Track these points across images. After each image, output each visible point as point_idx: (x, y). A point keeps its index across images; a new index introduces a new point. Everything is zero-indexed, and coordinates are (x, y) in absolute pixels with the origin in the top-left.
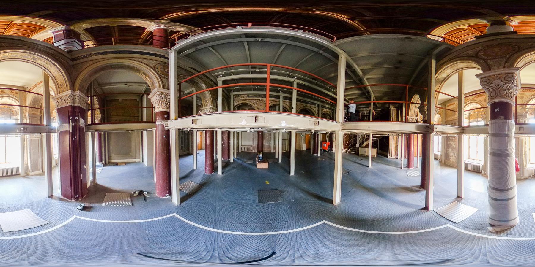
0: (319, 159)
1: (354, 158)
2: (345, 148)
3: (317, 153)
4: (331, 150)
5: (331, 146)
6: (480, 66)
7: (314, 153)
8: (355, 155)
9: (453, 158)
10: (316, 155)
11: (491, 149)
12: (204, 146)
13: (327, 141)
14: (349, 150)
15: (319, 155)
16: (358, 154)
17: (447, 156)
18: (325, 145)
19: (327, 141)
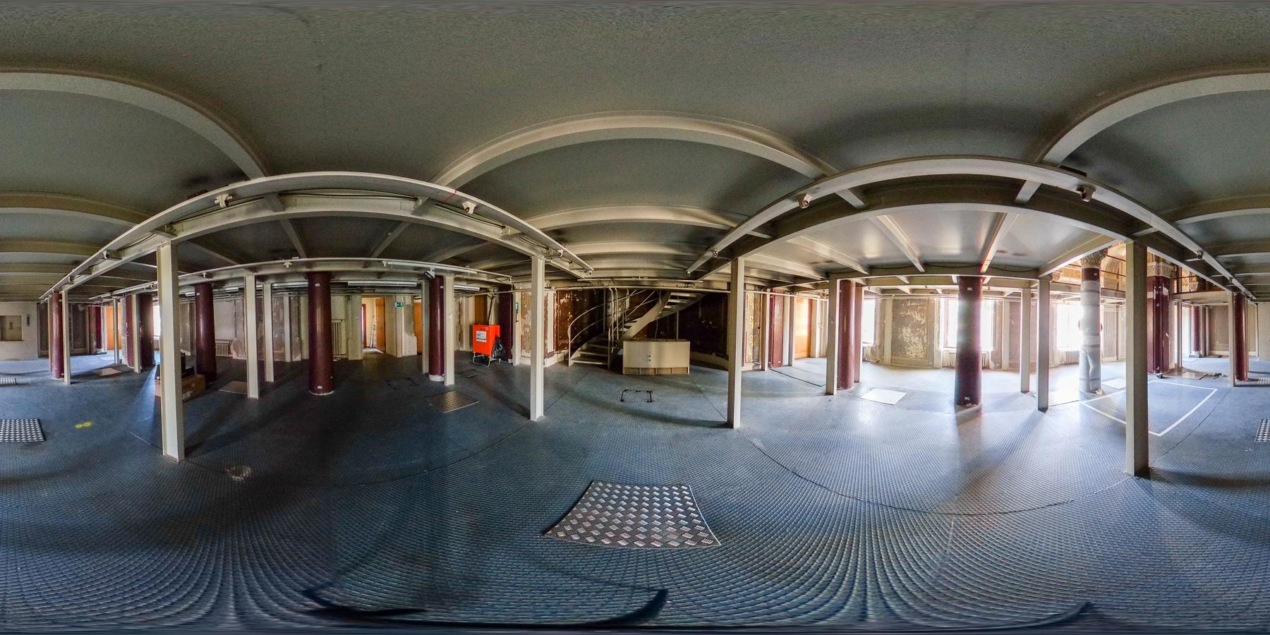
0: (451, 398)
1: (608, 389)
2: (558, 347)
3: (442, 372)
4: (507, 354)
5: (505, 339)
6: (832, 629)
7: (432, 372)
8: (603, 373)
9: (915, 350)
10: (436, 378)
11: (260, 176)
12: (854, 289)
13: (492, 320)
14: (577, 354)
15: (450, 379)
16: (615, 365)
17: (898, 346)
18: (482, 336)
19: (492, 320)
